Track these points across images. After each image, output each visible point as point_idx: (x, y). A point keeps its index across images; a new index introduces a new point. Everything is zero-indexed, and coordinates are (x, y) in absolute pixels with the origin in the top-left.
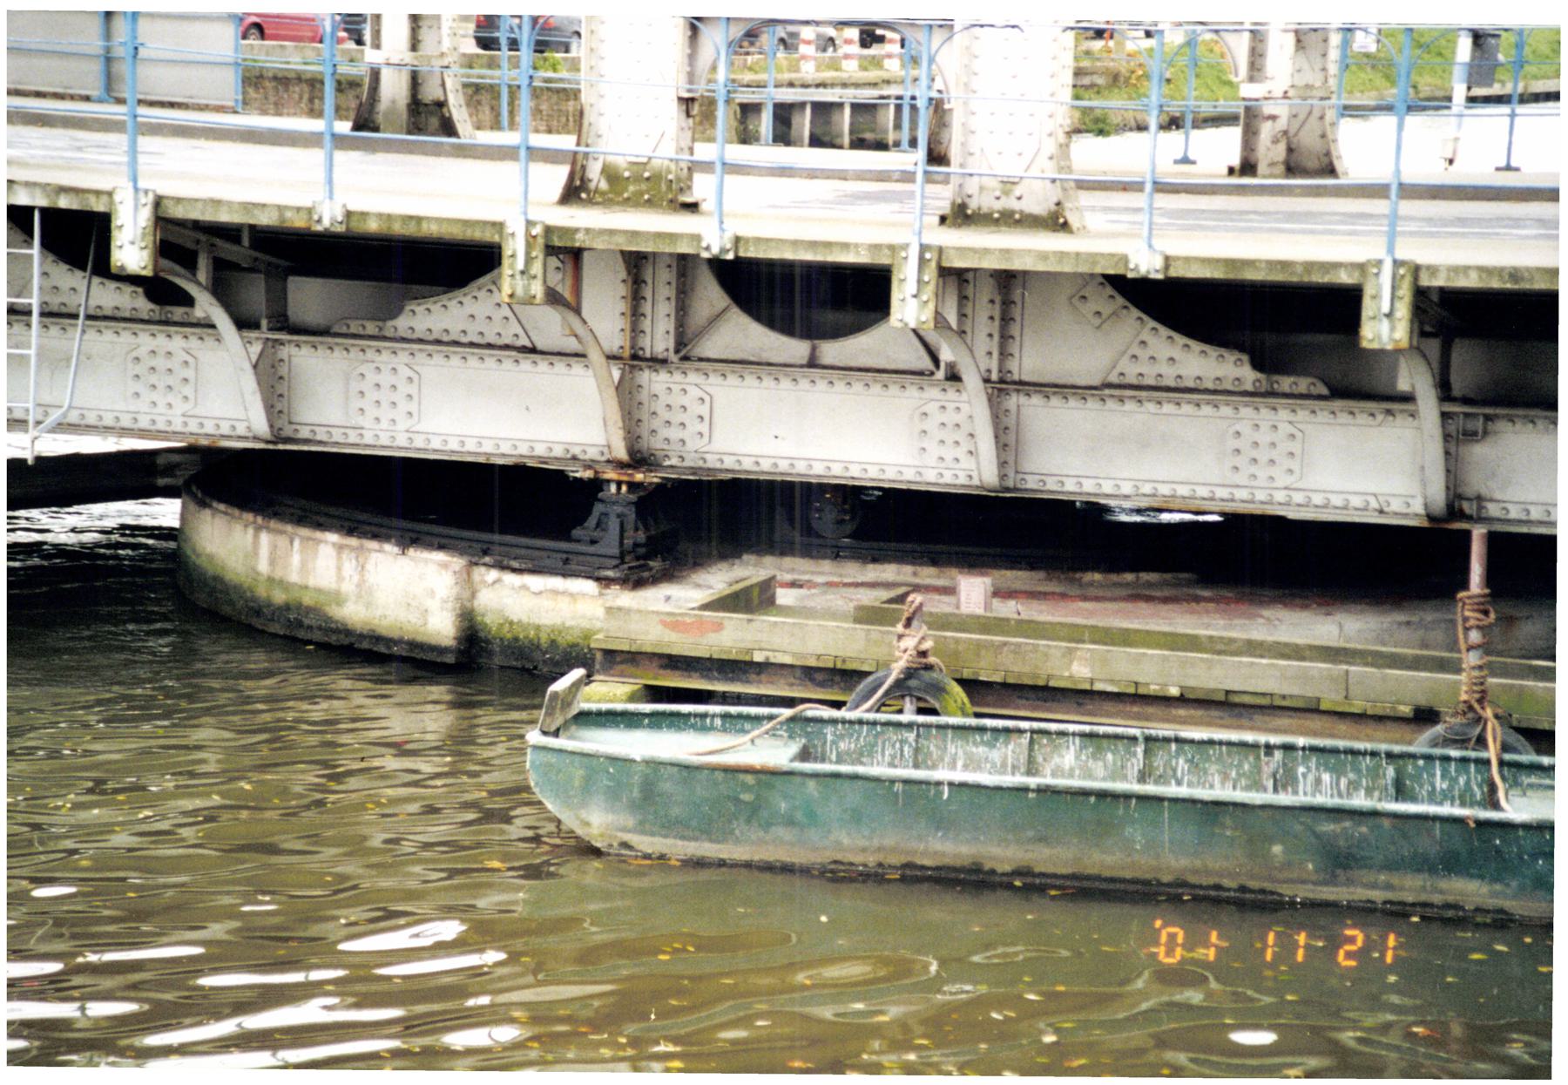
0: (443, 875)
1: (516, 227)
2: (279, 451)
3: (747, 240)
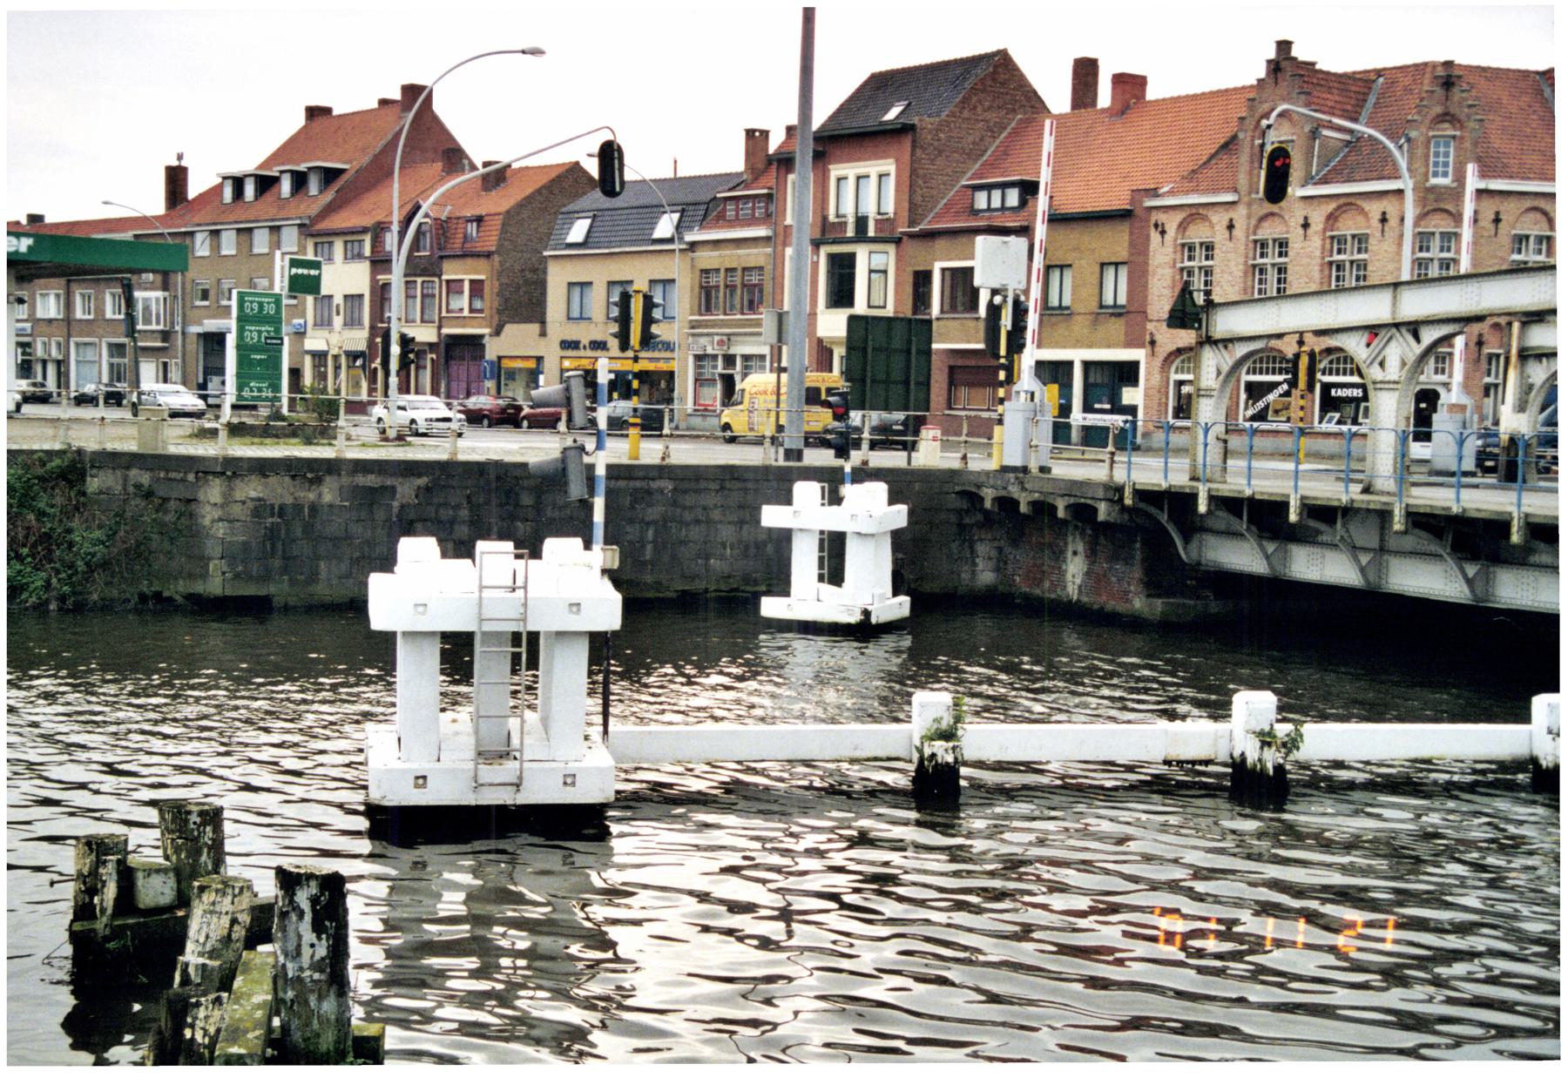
1: (1515, 515)
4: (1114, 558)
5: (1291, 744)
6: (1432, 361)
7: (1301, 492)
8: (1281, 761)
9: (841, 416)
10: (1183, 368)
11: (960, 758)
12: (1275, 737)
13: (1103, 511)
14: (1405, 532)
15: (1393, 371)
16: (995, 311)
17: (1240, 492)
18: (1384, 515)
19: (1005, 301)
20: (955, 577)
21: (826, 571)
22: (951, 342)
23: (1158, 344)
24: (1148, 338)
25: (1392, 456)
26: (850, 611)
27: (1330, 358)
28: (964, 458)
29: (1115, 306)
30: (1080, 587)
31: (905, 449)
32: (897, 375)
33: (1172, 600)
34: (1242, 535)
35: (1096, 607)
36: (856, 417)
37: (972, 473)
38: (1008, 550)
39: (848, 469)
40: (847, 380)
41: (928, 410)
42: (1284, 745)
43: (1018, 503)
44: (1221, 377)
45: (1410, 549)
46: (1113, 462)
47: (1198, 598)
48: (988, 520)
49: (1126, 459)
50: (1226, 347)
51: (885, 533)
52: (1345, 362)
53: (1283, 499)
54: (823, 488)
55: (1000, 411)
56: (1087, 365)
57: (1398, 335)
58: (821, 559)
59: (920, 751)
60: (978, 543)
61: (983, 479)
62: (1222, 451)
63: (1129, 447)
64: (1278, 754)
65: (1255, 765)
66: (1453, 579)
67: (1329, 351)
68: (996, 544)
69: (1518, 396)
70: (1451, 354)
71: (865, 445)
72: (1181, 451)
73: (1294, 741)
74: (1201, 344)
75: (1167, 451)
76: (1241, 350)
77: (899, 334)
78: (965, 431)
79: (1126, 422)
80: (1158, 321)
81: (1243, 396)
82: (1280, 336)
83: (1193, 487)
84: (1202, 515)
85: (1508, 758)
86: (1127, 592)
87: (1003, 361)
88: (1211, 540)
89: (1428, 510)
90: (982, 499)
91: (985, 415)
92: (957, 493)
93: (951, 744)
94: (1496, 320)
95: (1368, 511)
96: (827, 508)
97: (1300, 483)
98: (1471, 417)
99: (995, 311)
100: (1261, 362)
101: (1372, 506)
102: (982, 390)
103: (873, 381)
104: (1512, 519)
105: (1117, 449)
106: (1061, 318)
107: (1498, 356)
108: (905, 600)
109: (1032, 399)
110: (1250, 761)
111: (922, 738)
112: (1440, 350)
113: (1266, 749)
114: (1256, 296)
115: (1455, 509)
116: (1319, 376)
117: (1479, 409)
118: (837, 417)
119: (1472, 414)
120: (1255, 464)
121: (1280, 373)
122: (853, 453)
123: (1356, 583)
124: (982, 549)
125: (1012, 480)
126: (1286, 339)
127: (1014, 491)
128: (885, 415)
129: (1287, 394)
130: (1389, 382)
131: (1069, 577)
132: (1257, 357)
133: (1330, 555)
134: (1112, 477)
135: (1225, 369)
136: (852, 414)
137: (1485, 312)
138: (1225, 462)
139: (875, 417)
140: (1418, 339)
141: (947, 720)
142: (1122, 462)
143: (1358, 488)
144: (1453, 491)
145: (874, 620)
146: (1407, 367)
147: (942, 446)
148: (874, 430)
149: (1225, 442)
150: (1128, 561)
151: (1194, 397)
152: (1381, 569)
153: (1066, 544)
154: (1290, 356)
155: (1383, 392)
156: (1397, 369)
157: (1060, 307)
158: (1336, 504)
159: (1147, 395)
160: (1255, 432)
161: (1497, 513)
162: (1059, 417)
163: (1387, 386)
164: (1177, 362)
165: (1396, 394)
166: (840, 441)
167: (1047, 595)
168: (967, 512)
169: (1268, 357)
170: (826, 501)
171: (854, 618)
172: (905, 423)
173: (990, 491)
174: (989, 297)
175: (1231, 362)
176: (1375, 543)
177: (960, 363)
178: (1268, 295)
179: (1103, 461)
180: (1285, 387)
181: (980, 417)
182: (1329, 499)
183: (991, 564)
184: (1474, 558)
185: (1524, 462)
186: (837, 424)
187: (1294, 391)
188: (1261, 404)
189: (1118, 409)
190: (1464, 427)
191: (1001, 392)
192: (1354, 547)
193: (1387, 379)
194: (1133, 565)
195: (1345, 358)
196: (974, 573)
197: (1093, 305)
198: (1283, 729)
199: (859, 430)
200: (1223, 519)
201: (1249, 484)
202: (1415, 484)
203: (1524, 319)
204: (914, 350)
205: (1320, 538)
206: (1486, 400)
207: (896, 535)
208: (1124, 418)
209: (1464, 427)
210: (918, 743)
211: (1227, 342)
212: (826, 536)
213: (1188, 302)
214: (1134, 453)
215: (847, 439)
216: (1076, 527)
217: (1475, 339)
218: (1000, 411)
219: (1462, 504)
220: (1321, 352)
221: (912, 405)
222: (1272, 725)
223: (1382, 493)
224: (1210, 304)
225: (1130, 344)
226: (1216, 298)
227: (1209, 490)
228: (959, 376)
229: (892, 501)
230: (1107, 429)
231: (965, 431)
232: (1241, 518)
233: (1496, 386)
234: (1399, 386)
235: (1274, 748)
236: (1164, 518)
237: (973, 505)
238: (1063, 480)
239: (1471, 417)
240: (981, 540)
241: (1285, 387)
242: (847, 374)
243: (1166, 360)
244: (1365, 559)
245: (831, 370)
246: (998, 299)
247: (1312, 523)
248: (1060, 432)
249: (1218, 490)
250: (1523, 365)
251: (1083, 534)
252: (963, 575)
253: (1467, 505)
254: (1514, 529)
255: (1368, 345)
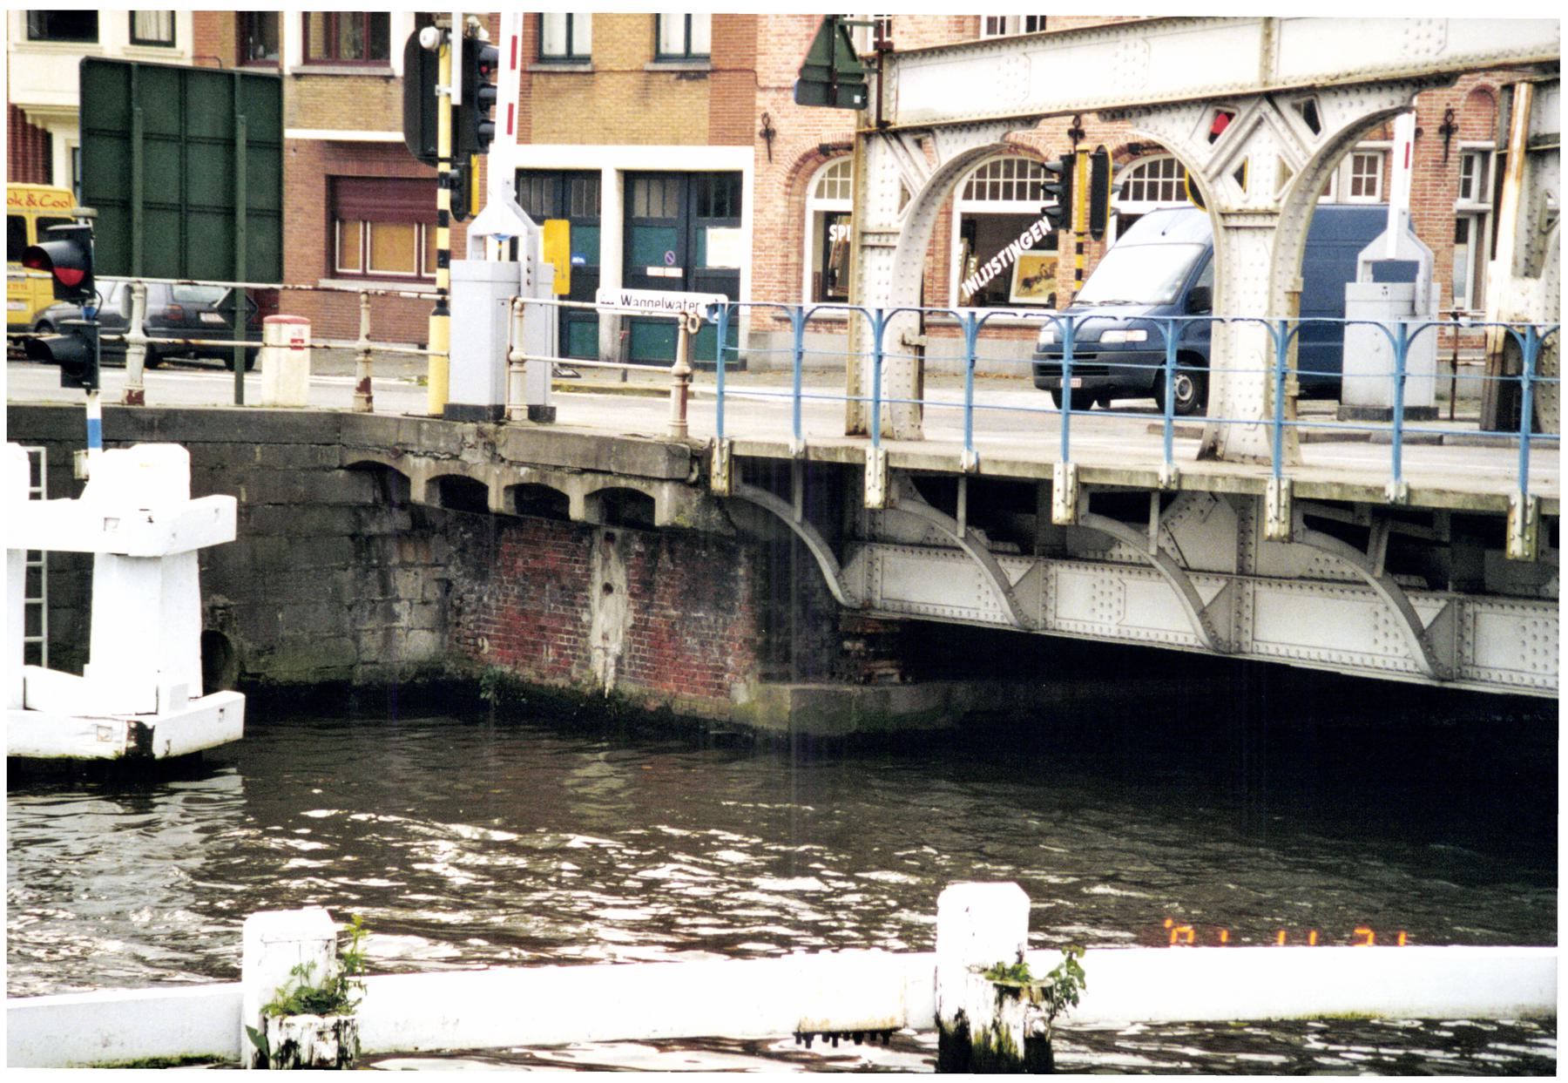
0: (1342, 1055)
1: (1517, 500)
2: (1446, 690)
3: (894, 455)
4: (691, 596)
5: (1060, 993)
6: (1347, 162)
7: (1076, 459)
8: (1041, 1027)
9: (74, 289)
10: (832, 185)
11: (351, 1050)
12: (1027, 978)
13: (667, 506)
14: (1290, 538)
15: (1263, 191)
16: (423, 63)
17: (950, 460)
18: (1245, 506)
19: (445, 40)
20: (348, 642)
21: (43, 638)
22: (333, 126)
23: (779, 137)
24: (759, 126)
25: (1261, 377)
26: (102, 730)
27: (1137, 164)
28: (365, 386)
29: (688, 55)
30: (619, 660)
31: (230, 367)
32: (204, 191)
33: (813, 686)
34: (959, 549)
35: (653, 705)
36: (109, 291)
37: (384, 420)
38: (462, 585)
39: (94, 413)
40: (86, 202)
41: (279, 278)
42: (1047, 993)
43: (482, 489)
44: (911, 204)
45: (1298, 572)
46: (686, 395)
47: (868, 680)
48: (420, 525)
49: (714, 390)
50: (919, 143)
51: (185, 554)
52: (1168, 173)
53: (1039, 474)
54: (34, 459)
55: (442, 283)
56: (630, 179)
57: (1273, 115)
58: (32, 612)
59: (260, 1039)
60: (399, 573)
61: (406, 436)
62: (913, 369)
63: (720, 362)
64: (1033, 1013)
65: (987, 1038)
66: (1392, 629)
67: (1134, 149)
68: (439, 572)
69: (1524, 239)
70: (1386, 152)
71: (135, 357)
72: (830, 370)
73: (1067, 985)
74: (868, 136)
75: (799, 369)
76: (950, 149)
77: (206, 117)
78: (365, 327)
79: (713, 308)
80: (779, 89)
81: (958, 247)
82: (1030, 121)
83: (850, 450)
84: (873, 511)
85: (1292, 1018)
86: (720, 670)
87: (444, 167)
88: (890, 558)
89: (1336, 495)
90: (405, 481)
91: (408, 290)
92: (354, 468)
93: (331, 1020)
94: (1482, 80)
95: (1214, 496)
96: (44, 502)
97: (1074, 440)
98: (1428, 291)
99: (423, 63)
100: (995, 173)
101: (1220, 488)
102: (404, 232)
103: (148, 206)
104: (1510, 508)
105: (695, 366)
106: (572, 79)
107: (1485, 154)
108: (233, 702)
109: (513, 256)
110: (975, 1030)
111: (265, 1010)
112: (1362, 144)
113: (1008, 1001)
114: (984, 36)
115: (1393, 492)
116: (1113, 201)
117: (1444, 267)
118: (64, 291)
119: (1428, 281)
120: (980, 397)
121: (1035, 197)
122: (106, 376)
123: (1191, 641)
124: (408, 584)
125: (470, 439)
126: (1044, 125)
127: (476, 465)
128: (182, 290)
129: (1050, 242)
130: (1254, 213)
131: (595, 639)
132: (987, 162)
133: (1136, 584)
134: (684, 428)
135: (918, 187)
136: (102, 284)
137: (1455, 66)
138: (920, 395)
139: (158, 294)
140: (1314, 124)
141: (325, 970)
142: (707, 396)
143: (1193, 447)
144: (1388, 451)
145: (159, 751)
146: (1291, 182)
147: (313, 361)
148: (158, 322)
149: (920, 349)
150: (722, 601)
151: (854, 251)
152: (1241, 612)
153: (588, 572)
154: (1054, 161)
155: (1245, 236)
156: (1272, 185)
157: (569, 57)
158: (1147, 483)
159: (758, 248)
160: (981, 327)
161: (1478, 497)
162: (570, 297)
163: (1249, 222)
164: (821, 173)
165: (1270, 238)
166: (77, 348)
167: (548, 681)
168: (375, 507)
169: (1009, 163)
170: (43, 489)
171: (114, 745)
172: (227, 308)
173: (422, 462)
174: (411, 28)
175: (929, 175)
176: (1229, 562)
177: (351, 169)
178: (1009, 33)
179: (666, 393)
180: (1045, 225)
181: (398, 297)
182: (1132, 474)
183: (428, 615)
184: (1434, 584)
185: (1533, 384)
186: (67, 308)
187: (1062, 234)
188: (994, 267)
189: (695, 278)
190: (1413, 314)
191: (443, 238)
192: (1186, 568)
193: (1251, 206)
194: (730, 611)
195: (1169, 163)
196: (388, 634)
197: (640, 55)
198: (1043, 965)
199: (118, 323)
200: (918, 516)
201: (969, 443)
202: (1308, 439)
203: (1540, 78)
204: (241, 142)
205: (1116, 552)
206: (1460, 248)
207: (212, 562)
208: (711, 298)
209: (1413, 314)
210: (255, 1022)
211: (922, 133)
212: (43, 563)
213: (840, 49)
214: (729, 376)
215: (90, 343)
216: (610, 538)
217: (1438, 122)
218: (442, 283)
219: (1405, 478)
220: (1119, 152)
221: (241, 266)
222: (1020, 955)
223: (1243, 459)
224: (885, 53)
225: (721, 136)
226: (900, 42)
227: (887, 456)
228: (348, 199)
229: (200, 487)
230: (672, 323)
231: (365, 327)
232: (954, 515)
233: (1481, 216)
234: (1275, 222)
235: (1025, 1000)
236: (794, 516)
237: (386, 497)
238: (581, 437)
239: (1428, 291)
240: (405, 565)
241: (1045, 225)
242: (85, 188)
243: (797, 169)
244: (1207, 591)
245: (48, 178)
246: (429, 37)
247: (1099, 523)
248: (575, 328)
249: (904, 456)
250: (1534, 173)
251: (624, 555)
252: (366, 640)
253: (1415, 483)
254: (1514, 529)
255: (1213, 137)
